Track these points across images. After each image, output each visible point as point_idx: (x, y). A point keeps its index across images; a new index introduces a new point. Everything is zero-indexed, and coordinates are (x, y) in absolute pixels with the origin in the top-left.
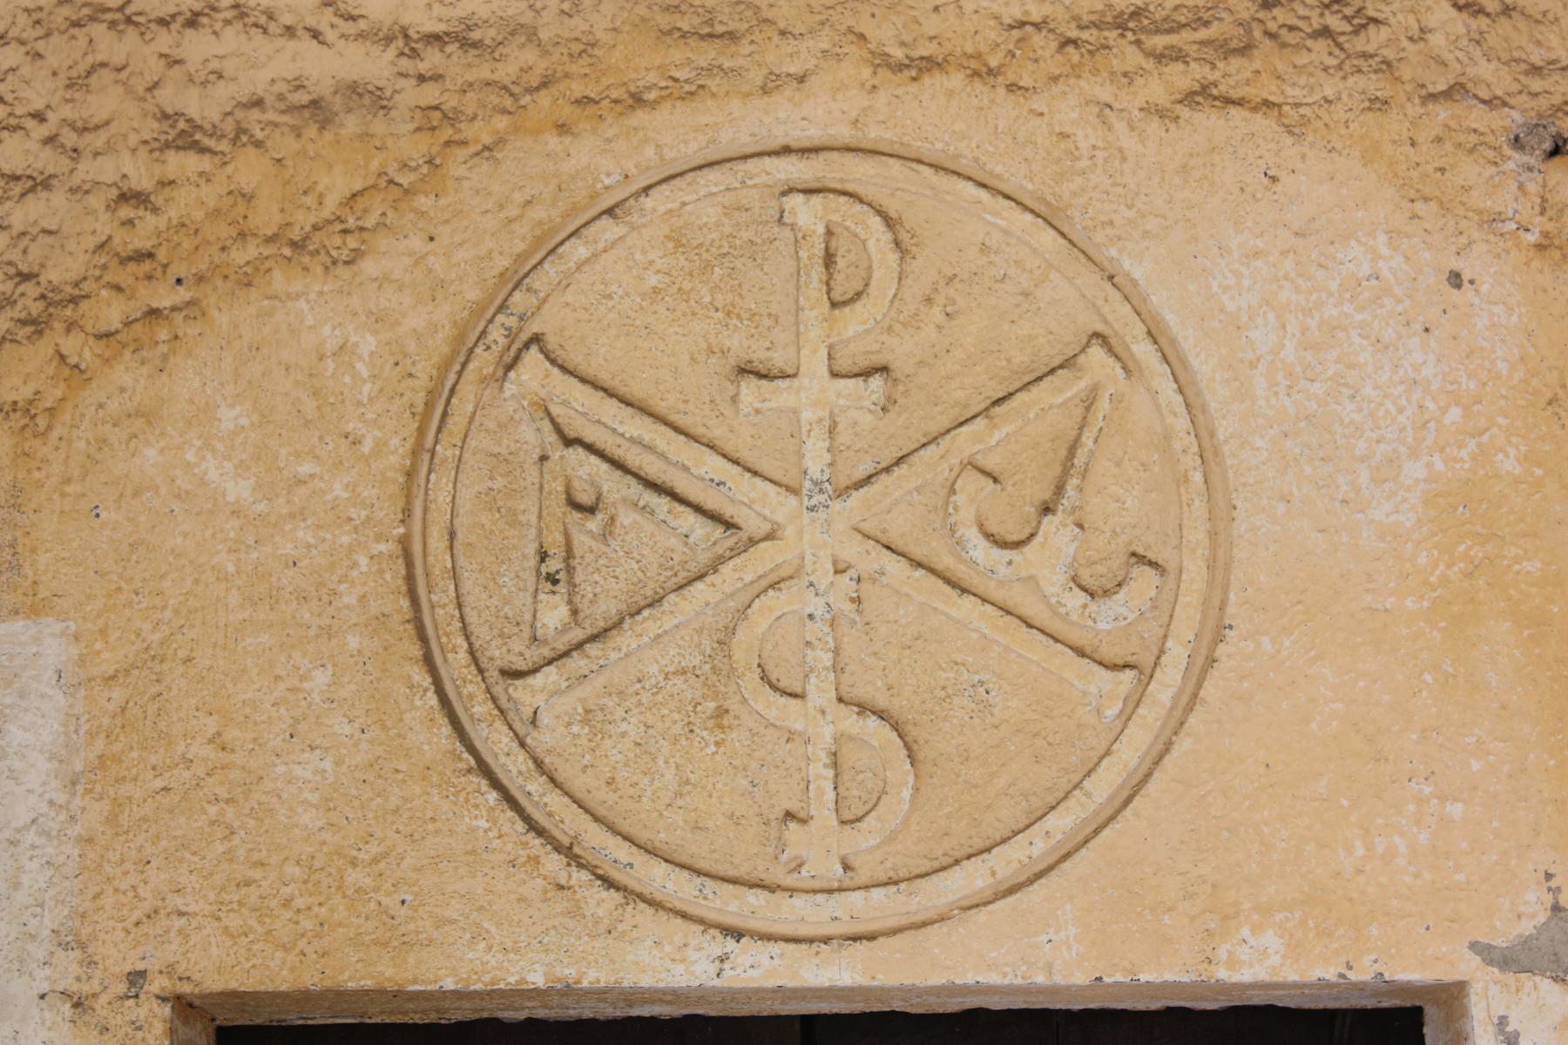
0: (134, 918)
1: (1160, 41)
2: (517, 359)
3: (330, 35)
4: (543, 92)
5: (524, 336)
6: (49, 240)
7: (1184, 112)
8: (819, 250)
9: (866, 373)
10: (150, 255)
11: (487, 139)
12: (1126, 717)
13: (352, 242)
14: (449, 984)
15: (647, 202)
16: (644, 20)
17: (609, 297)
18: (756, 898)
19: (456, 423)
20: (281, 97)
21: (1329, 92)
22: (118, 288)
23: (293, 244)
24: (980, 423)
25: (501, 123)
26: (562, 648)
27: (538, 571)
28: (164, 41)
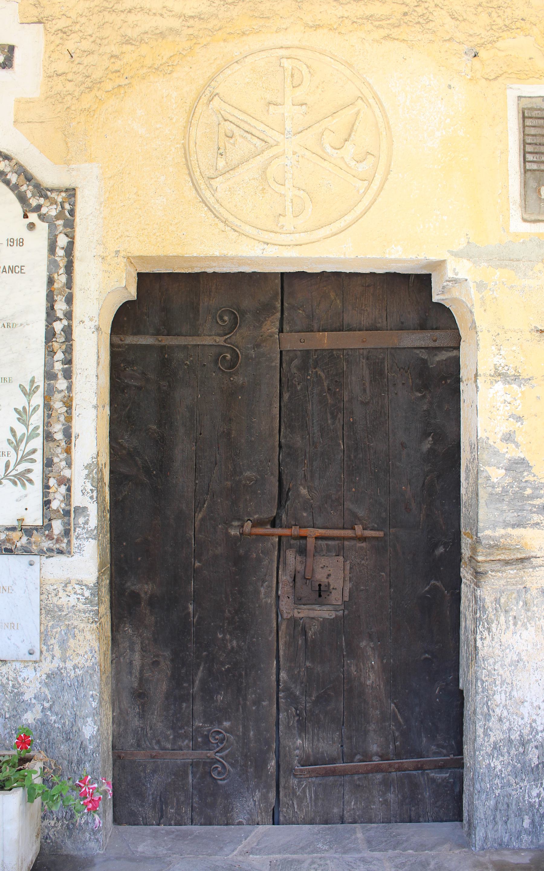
0: (116, 238)
1: (377, 23)
2: (212, 99)
3: (165, 16)
4: (220, 31)
5: (214, 94)
6: (94, 67)
7: (383, 41)
8: (290, 73)
9: (302, 105)
10: (119, 71)
11: (205, 43)
12: (365, 193)
13: (170, 68)
14: (195, 255)
15: (246, 60)
16: (246, 13)
17: (236, 84)
18: (272, 235)
19: (197, 115)
20: (152, 31)
21: (420, 38)
22: (111, 79)
23: (155, 69)
24: (330, 118)
25: (209, 39)
26: (224, 172)
27: (218, 153)
28: (123, 16)
